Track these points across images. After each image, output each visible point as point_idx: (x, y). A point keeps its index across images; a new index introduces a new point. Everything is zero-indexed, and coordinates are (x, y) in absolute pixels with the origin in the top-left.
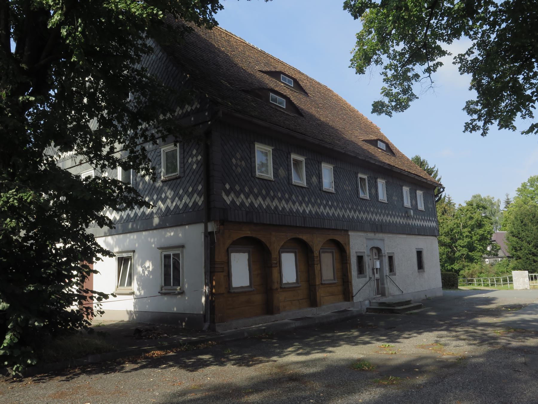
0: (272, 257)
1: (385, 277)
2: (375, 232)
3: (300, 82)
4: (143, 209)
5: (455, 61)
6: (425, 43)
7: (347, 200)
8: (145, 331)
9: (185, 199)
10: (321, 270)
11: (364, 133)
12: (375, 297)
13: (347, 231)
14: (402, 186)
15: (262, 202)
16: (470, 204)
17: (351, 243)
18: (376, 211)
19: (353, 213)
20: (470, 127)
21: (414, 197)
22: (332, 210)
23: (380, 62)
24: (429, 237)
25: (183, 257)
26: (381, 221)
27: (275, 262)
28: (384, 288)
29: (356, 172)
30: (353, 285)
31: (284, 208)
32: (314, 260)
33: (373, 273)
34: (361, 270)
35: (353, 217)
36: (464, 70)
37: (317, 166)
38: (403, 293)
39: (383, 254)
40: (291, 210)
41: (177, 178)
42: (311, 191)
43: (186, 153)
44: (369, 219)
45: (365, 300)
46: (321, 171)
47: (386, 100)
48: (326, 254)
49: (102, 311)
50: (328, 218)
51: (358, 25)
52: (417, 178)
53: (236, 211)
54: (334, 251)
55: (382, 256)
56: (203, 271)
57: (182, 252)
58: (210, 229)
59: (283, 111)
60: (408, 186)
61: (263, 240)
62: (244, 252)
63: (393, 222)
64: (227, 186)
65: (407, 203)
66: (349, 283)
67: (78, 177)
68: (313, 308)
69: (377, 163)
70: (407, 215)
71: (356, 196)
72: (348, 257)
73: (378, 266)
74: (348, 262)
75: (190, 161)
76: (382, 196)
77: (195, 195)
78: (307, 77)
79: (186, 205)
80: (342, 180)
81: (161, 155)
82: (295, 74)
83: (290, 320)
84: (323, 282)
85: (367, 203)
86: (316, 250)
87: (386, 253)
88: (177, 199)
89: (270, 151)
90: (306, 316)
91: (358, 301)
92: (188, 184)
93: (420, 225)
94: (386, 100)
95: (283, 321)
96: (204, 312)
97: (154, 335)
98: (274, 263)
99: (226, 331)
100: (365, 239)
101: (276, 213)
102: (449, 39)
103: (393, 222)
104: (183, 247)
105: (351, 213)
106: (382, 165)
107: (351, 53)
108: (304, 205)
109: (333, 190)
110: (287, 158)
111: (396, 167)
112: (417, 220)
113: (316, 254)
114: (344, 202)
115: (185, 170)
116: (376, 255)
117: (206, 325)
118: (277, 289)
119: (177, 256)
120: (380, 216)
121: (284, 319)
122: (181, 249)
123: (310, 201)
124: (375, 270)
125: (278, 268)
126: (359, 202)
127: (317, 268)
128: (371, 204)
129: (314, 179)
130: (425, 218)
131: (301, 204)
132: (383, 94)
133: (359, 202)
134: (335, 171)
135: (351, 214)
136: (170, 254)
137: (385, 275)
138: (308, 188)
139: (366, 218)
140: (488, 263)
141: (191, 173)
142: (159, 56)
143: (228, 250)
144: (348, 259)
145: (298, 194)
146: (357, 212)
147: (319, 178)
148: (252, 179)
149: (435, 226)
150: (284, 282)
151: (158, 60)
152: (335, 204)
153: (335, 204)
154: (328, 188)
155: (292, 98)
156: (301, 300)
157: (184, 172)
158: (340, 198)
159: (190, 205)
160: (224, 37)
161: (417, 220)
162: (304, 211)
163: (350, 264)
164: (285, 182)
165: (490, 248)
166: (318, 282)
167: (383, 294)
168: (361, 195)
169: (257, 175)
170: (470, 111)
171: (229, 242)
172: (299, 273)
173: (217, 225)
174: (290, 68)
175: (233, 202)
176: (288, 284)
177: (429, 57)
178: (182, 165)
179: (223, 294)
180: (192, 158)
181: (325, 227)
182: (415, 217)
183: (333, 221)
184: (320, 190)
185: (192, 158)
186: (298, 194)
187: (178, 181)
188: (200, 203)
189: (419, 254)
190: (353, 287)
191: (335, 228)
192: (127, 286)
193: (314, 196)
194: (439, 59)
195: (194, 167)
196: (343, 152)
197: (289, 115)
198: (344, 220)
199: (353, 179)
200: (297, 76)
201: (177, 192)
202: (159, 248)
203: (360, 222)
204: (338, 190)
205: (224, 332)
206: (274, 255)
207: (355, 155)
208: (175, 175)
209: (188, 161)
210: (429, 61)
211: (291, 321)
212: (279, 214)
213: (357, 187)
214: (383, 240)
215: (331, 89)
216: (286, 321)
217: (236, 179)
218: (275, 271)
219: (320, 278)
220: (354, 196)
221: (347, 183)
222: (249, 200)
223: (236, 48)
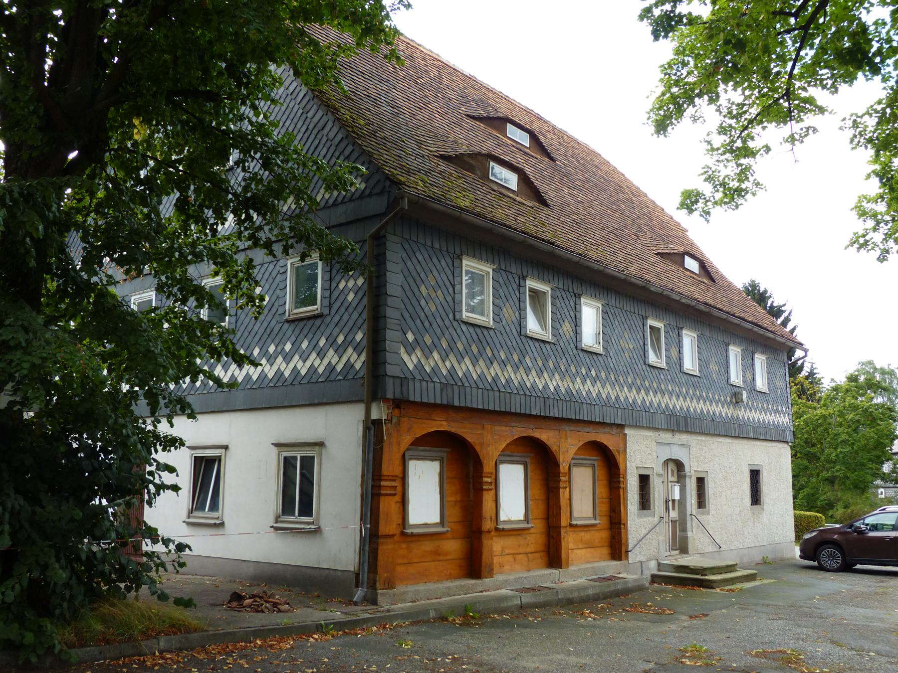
0: (485, 471)
1: (688, 517)
2: (673, 431)
3: (541, 137)
4: (248, 368)
5: (842, 124)
6: (788, 90)
7: (624, 368)
8: (250, 598)
9: (331, 356)
10: (570, 499)
11: (658, 239)
12: (668, 553)
13: (622, 426)
14: (727, 345)
15: (471, 368)
16: (853, 379)
17: (628, 450)
18: (678, 391)
19: (635, 392)
20: (861, 243)
21: (749, 367)
22: (596, 386)
23: (701, 119)
24: (774, 444)
25: (320, 464)
26: (685, 409)
27: (489, 480)
28: (686, 538)
29: (644, 314)
30: (629, 529)
31: (509, 381)
32: (560, 481)
33: (667, 509)
34: (645, 503)
35: (634, 401)
36: (859, 142)
37: (572, 303)
38: (721, 549)
39: (688, 474)
40: (522, 385)
41: (315, 317)
42: (559, 349)
43: (334, 272)
44: (664, 406)
45: (649, 560)
46: (580, 312)
47: (707, 189)
48: (582, 469)
49: (181, 561)
50: (589, 402)
51: (667, 48)
52: (756, 329)
53: (424, 383)
54: (596, 463)
55: (685, 476)
56: (359, 491)
57: (320, 455)
58: (374, 416)
59: (512, 195)
60: (739, 345)
61: (470, 438)
62: (433, 460)
63: (708, 412)
64: (410, 337)
65: (736, 377)
66: (622, 526)
67: (126, 303)
68: (554, 571)
69: (683, 301)
70: (734, 400)
71: (641, 361)
72: (621, 476)
73: (677, 497)
74: (622, 485)
75: (342, 285)
76: (690, 363)
77: (350, 350)
78: (554, 128)
79: (331, 368)
80: (616, 331)
81: (286, 272)
82: (532, 122)
83: (516, 590)
84: (574, 523)
85: (662, 376)
86: (565, 457)
87: (692, 472)
88: (314, 355)
89: (489, 272)
90: (540, 584)
91: (637, 560)
92: (337, 330)
93: (759, 419)
94: (707, 189)
95: (497, 591)
96: (357, 568)
97: (267, 605)
98: (487, 482)
99: (395, 606)
100: (655, 444)
101: (495, 388)
102: (833, 85)
103: (708, 412)
104: (321, 444)
105: (632, 394)
106: (694, 304)
107: (648, 97)
108: (546, 375)
109: (600, 349)
110: (520, 285)
111: (719, 309)
112: (753, 411)
113: (564, 468)
114: (618, 372)
115: (332, 303)
116: (673, 475)
117: (359, 594)
118: (489, 532)
119: (308, 463)
120: (685, 399)
121: (501, 589)
122: (317, 448)
123: (557, 368)
124: (670, 503)
125: (493, 492)
126: (646, 372)
127: (564, 494)
128: (669, 377)
129: (567, 327)
130: (768, 408)
131: (540, 374)
132: (704, 177)
133: (646, 372)
134: (605, 312)
135: (632, 395)
136: (296, 457)
137: (688, 513)
138: (554, 344)
139: (659, 404)
140: (883, 496)
141: (342, 310)
142: (291, 89)
143: (404, 456)
144: (621, 479)
145: (536, 354)
146: (643, 392)
147: (576, 326)
148: (455, 324)
149: (787, 424)
150: (502, 519)
151: (289, 96)
152: (603, 375)
153: (603, 375)
154: (591, 345)
155: (528, 170)
156: (532, 553)
157: (330, 306)
158: (612, 365)
159: (339, 368)
160: (403, 51)
161: (753, 411)
162: (546, 386)
163: (625, 489)
164: (514, 331)
165: (889, 467)
166: (564, 522)
167: (684, 549)
168: (652, 358)
169: (464, 317)
170: (863, 214)
171: (408, 439)
172: (530, 503)
173: (388, 408)
174: (528, 112)
175: (419, 366)
176: (509, 522)
177: (794, 116)
178: (327, 294)
179: (393, 536)
180: (347, 282)
181: (582, 418)
182: (750, 403)
183: (597, 407)
184: (576, 348)
185: (347, 282)
186: (536, 354)
187: (318, 322)
188: (358, 366)
189: (755, 475)
190: (629, 533)
191: (601, 421)
192: (209, 511)
193: (564, 359)
194: (809, 119)
195: (351, 297)
196: (623, 277)
197: (524, 204)
198: (617, 406)
199: (638, 328)
200: (535, 127)
201: (314, 342)
202: (276, 445)
203: (647, 410)
204: (609, 348)
205: (392, 607)
206: (488, 467)
207: (644, 284)
208: (312, 311)
209: (337, 286)
210: (793, 122)
211: (515, 593)
212: (499, 391)
213: (680, 366)
214: (687, 446)
215: (607, 159)
216: (504, 592)
217: (427, 324)
218: (487, 499)
219: (568, 514)
220: (637, 361)
221: (627, 337)
222: (448, 364)
223: (426, 71)
